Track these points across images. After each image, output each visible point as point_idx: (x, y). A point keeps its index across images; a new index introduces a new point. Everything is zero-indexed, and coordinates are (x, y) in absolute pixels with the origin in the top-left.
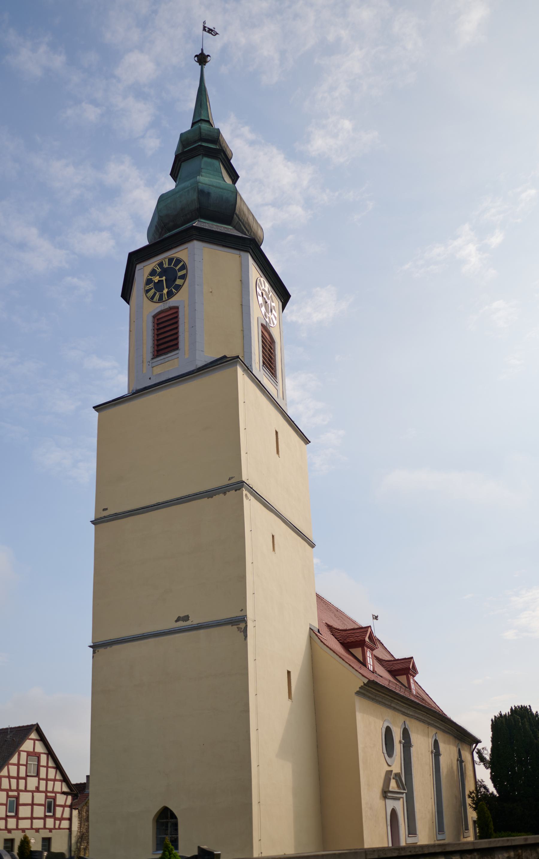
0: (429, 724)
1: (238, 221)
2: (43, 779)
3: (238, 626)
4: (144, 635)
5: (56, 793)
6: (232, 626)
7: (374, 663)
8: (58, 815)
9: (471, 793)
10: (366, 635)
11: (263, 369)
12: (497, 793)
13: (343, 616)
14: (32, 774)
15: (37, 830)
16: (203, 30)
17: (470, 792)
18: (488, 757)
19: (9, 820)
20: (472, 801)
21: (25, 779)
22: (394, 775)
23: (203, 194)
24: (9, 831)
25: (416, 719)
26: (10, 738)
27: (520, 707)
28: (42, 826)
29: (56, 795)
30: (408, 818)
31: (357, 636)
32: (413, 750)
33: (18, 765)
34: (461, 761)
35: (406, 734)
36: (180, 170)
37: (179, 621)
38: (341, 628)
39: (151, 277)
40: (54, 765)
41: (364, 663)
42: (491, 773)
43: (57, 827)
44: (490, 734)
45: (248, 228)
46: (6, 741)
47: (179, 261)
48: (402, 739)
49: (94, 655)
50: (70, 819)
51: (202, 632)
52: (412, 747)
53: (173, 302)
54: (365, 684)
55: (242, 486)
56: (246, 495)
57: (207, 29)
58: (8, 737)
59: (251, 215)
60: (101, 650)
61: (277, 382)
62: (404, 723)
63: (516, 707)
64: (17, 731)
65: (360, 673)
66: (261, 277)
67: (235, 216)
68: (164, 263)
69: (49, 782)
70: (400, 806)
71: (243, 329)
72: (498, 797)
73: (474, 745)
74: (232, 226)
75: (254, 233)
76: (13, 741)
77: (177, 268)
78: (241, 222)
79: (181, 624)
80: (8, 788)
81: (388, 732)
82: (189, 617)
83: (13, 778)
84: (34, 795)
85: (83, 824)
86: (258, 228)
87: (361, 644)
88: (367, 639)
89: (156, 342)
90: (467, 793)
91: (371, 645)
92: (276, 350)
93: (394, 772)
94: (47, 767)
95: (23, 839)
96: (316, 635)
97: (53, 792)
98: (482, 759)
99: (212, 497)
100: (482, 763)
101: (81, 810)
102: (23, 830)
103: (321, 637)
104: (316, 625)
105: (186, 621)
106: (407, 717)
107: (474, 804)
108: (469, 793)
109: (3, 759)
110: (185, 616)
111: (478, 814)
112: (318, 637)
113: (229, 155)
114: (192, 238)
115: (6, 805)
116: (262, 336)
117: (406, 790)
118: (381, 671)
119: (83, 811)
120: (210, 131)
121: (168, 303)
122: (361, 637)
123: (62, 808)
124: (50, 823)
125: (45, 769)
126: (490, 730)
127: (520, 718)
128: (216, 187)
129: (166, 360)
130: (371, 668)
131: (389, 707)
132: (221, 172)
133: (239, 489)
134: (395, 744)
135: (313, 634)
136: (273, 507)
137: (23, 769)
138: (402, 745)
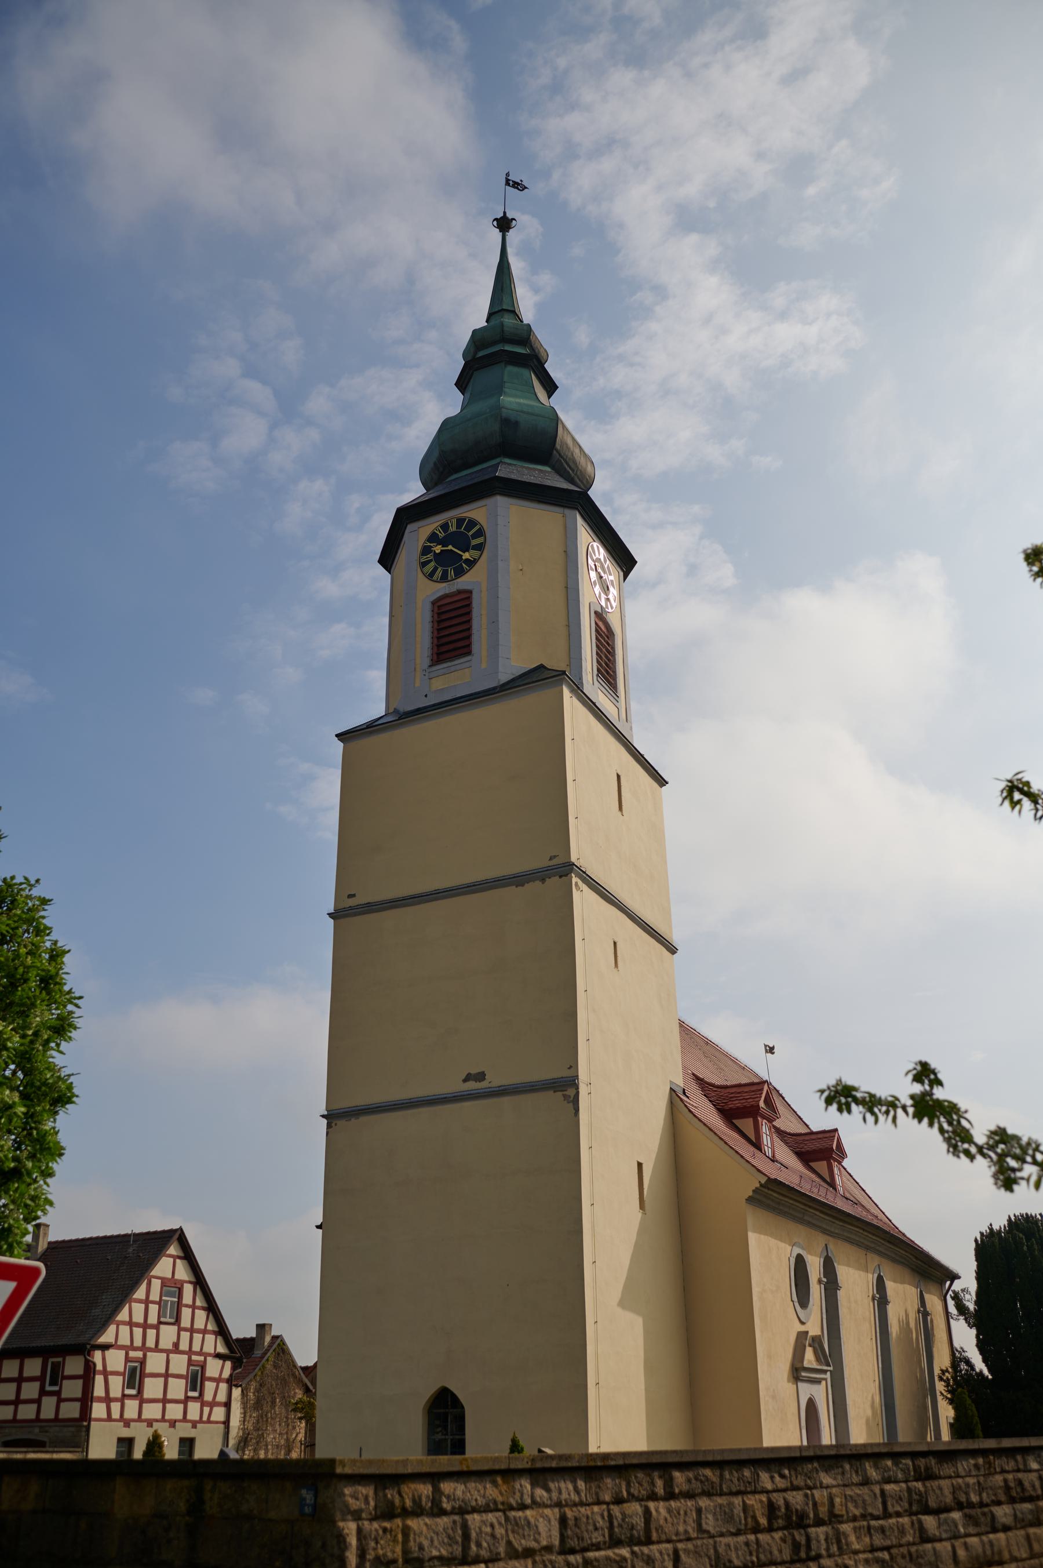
0: (868, 1248)
1: (558, 459)
2: (185, 1330)
3: (565, 1093)
4: (412, 1100)
5: (206, 1355)
6: (555, 1092)
7: (773, 1142)
8: (208, 1396)
9: (943, 1372)
10: (761, 1097)
11: (598, 681)
12: (989, 1373)
13: (717, 1054)
14: (168, 1320)
15: (173, 1423)
16: (506, 185)
17: (942, 1370)
18: (971, 1306)
19: (127, 1402)
20: (945, 1387)
21: (156, 1327)
22: (811, 1339)
23: (508, 424)
24: (127, 1423)
25: (846, 1240)
26: (133, 1254)
27: (1024, 1215)
28: (180, 1416)
29: (205, 1359)
30: (834, 1416)
31: (745, 1097)
32: (841, 1294)
33: (147, 1302)
34: (924, 1313)
35: (829, 1268)
36: (472, 380)
37: (469, 1081)
38: (717, 1083)
39: (429, 544)
40: (205, 1305)
41: (757, 1145)
42: (977, 1336)
43: (205, 1418)
44: (974, 1265)
45: (573, 466)
46: (126, 1257)
47: (472, 523)
48: (822, 1276)
49: (330, 1130)
50: (227, 1405)
51: (506, 1101)
52: (839, 1290)
53: (464, 582)
54: (761, 1185)
55: (571, 871)
56: (576, 884)
57: (511, 183)
58: (130, 1250)
59: (577, 446)
60: (341, 1123)
61: (618, 697)
62: (825, 1248)
63: (1018, 1216)
64: (144, 1240)
65: (753, 1166)
66: (594, 541)
67: (555, 452)
68: (450, 525)
69: (195, 1335)
70: (820, 1393)
71: (569, 623)
72: (992, 1379)
73: (948, 1283)
74: (549, 467)
75: (581, 471)
76: (138, 1258)
77: (471, 533)
78: (564, 459)
79: (472, 1085)
80: (128, 1343)
81: (800, 1265)
82: (485, 1075)
83: (138, 1325)
84: (170, 1358)
85: (248, 1415)
86: (587, 464)
87: (753, 1112)
88: (762, 1104)
89: (435, 648)
90: (937, 1372)
91: (768, 1113)
92: (616, 646)
93: (810, 1334)
94: (193, 1307)
95: (151, 1438)
96: (681, 1100)
97: (200, 1353)
98: (961, 1309)
99: (523, 885)
100: (962, 1318)
101: (246, 1389)
102: (150, 1423)
103: (689, 1104)
104: (680, 1081)
105: (480, 1082)
106: (831, 1238)
107: (949, 1391)
108: (941, 1372)
109: (122, 1291)
110: (479, 1073)
111: (956, 1409)
112: (684, 1104)
113: (543, 357)
114: (494, 492)
115: (123, 1374)
116: (597, 631)
117: (830, 1366)
118: (785, 1155)
119: (250, 1390)
120: (517, 329)
121: (456, 584)
122: (751, 1100)
123: (216, 1383)
124: (194, 1408)
125: (190, 1310)
126: (974, 1258)
127: (1024, 1237)
128: (528, 413)
129: (453, 669)
130: (769, 1153)
131: (801, 1221)
132: (532, 386)
133: (566, 875)
134: (811, 1286)
135: (676, 1099)
136: (615, 898)
137: (154, 1309)
138: (823, 1286)
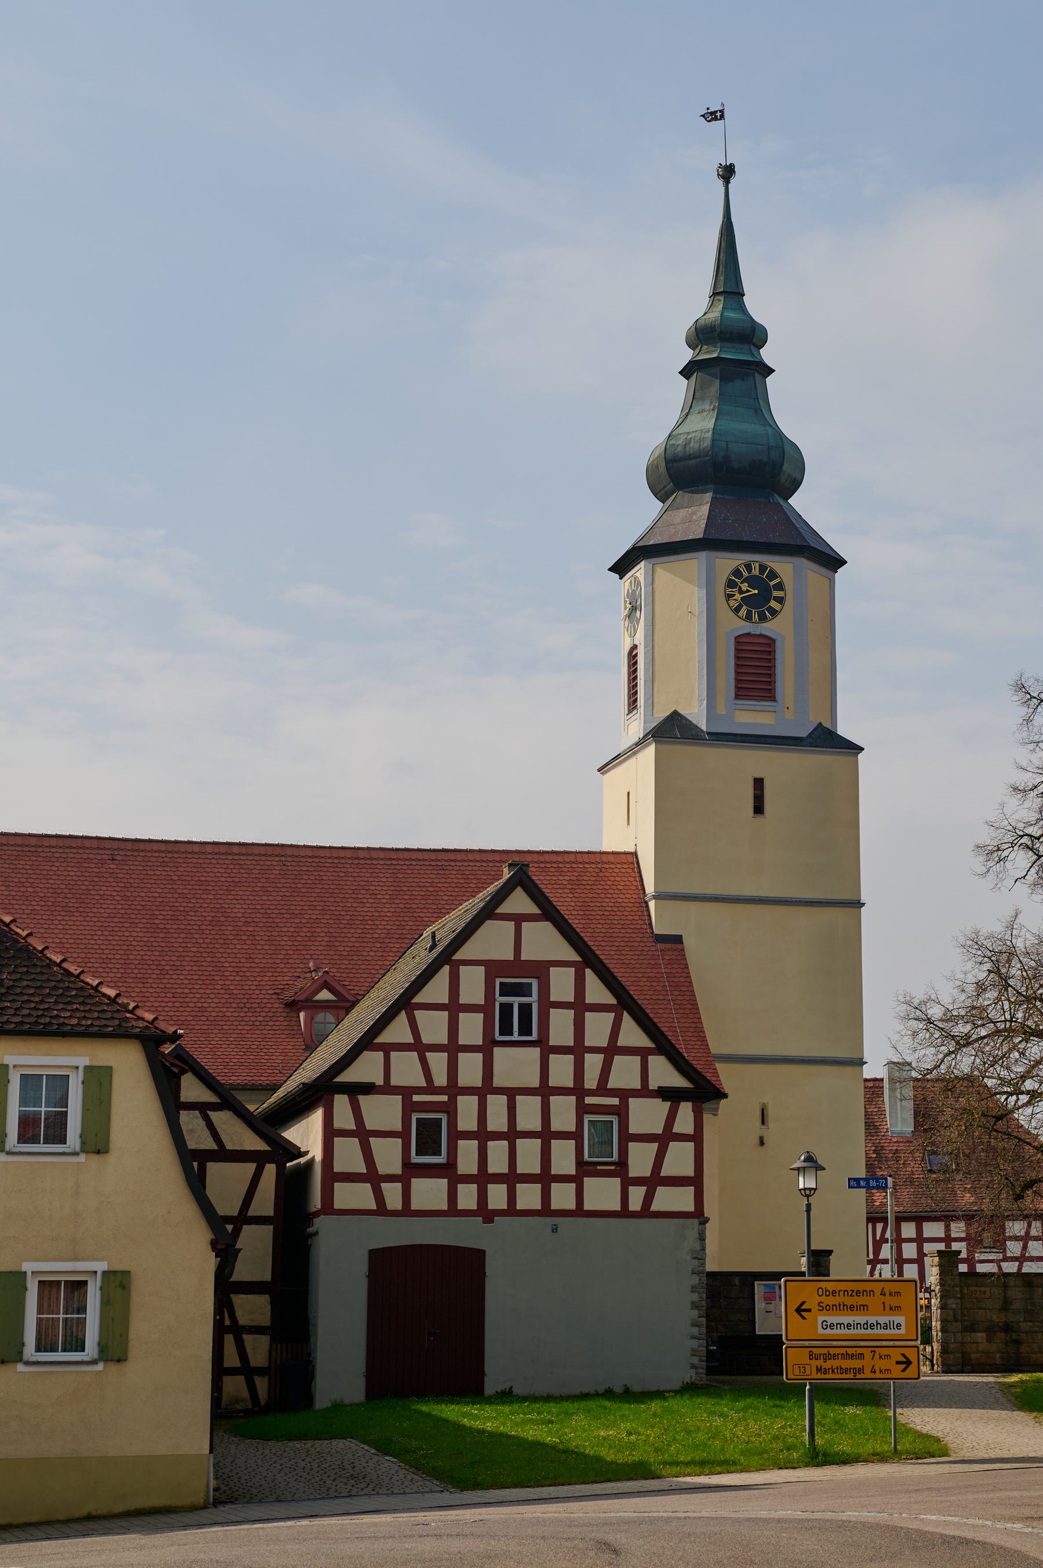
5: (625, 1095)
39: (734, 578)
47: (773, 575)
53: (768, 628)
77: (772, 583)
